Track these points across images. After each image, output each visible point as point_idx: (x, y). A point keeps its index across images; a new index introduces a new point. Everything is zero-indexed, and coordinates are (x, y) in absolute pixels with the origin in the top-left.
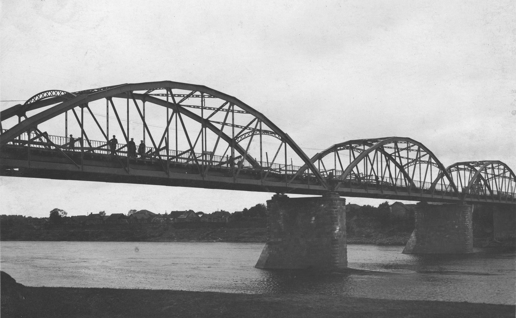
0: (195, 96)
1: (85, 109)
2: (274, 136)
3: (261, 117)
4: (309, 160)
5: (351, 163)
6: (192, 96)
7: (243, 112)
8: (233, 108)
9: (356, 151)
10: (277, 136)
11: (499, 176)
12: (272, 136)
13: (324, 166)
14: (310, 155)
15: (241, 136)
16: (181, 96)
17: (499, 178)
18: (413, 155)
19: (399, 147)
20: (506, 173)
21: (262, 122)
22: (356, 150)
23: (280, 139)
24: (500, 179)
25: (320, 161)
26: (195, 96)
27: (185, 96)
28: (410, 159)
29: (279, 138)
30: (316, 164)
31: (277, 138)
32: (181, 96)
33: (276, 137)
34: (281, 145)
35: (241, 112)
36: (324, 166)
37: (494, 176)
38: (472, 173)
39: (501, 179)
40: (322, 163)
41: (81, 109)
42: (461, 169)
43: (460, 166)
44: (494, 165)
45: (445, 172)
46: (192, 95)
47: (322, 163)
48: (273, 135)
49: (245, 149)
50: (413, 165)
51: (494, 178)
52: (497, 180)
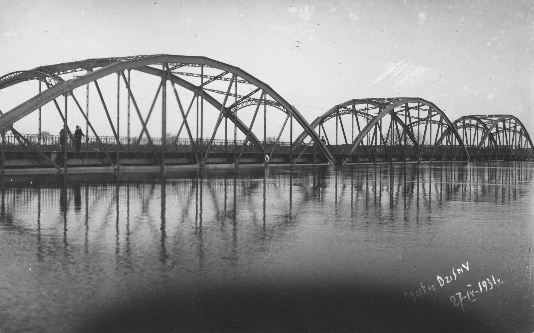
0: (223, 79)
1: (70, 98)
2: (277, 108)
3: (266, 89)
4: (308, 126)
5: (367, 134)
6: (220, 78)
7: (244, 82)
8: (266, 97)
9: (360, 116)
10: (282, 108)
11: (509, 129)
12: (276, 107)
13: (324, 132)
14: (310, 120)
15: (242, 103)
16: (208, 77)
17: (510, 132)
18: (424, 115)
19: (409, 106)
20: (517, 127)
21: (267, 95)
22: (360, 114)
23: (285, 112)
24: (511, 133)
25: (321, 126)
26: (223, 79)
27: (212, 78)
28: (206, 77)
29: (283, 110)
30: (316, 130)
31: (282, 110)
32: (208, 77)
33: (280, 109)
34: (287, 119)
35: (242, 82)
36: (324, 132)
37: (504, 129)
38: (522, 135)
39: (512, 133)
40: (323, 128)
41: (64, 97)
42: (470, 126)
43: (467, 122)
44: (411, 105)
45: (452, 129)
46: (220, 77)
47: (323, 128)
48: (277, 106)
49: (249, 127)
50: (416, 125)
51: (504, 131)
52: (508, 133)
